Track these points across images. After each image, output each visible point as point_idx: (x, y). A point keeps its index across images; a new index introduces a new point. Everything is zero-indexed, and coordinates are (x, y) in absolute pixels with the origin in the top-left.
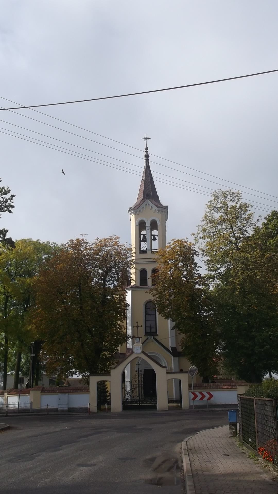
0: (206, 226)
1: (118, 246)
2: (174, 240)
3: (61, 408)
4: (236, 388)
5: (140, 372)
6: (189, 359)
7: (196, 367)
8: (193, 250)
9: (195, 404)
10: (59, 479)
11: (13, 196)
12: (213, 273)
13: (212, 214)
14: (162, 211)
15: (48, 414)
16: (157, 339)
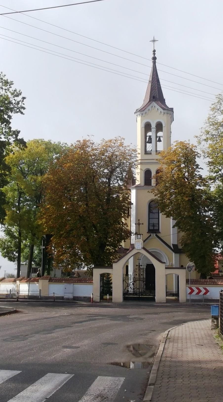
0: (209, 128)
1: (123, 147)
2: (177, 141)
3: (67, 296)
5: (140, 267)
6: (188, 256)
7: (193, 264)
8: (195, 152)
10: (42, 357)
11: (24, 98)
12: (214, 175)
13: (215, 116)
14: (168, 113)
15: (54, 301)
16: (159, 236)
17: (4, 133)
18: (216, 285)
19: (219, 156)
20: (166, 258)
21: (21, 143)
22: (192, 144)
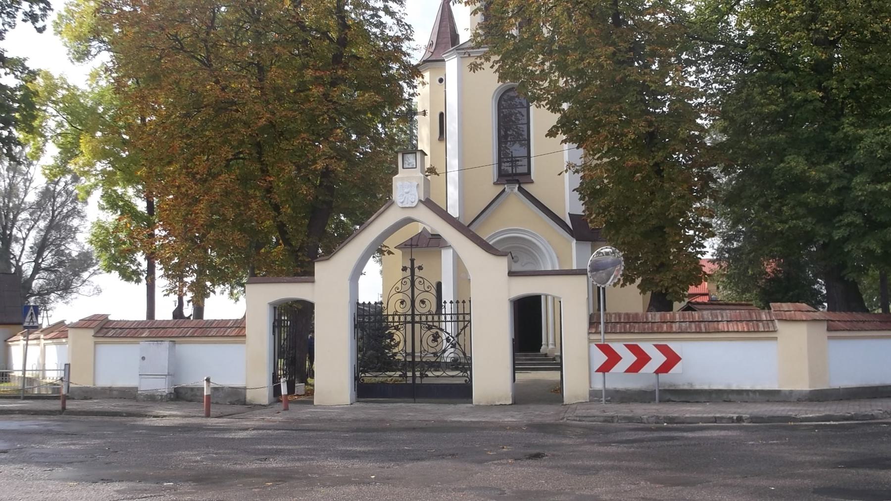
3: (147, 385)
4: (775, 331)
18: (706, 332)
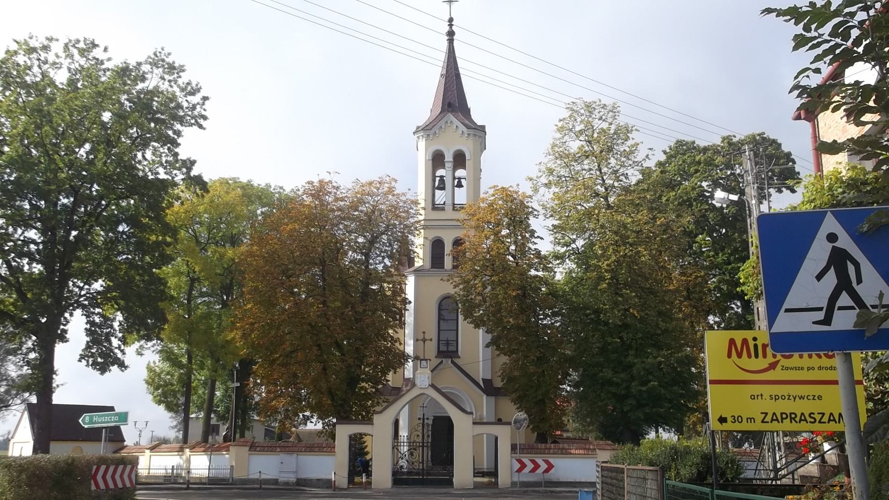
2: (494, 187)
3: (283, 478)
6: (514, 401)
7: (525, 415)
8: (528, 207)
9: (520, 480)
11: (205, 99)
12: (563, 250)
13: (565, 142)
14: (475, 135)
17: (165, 164)
19: (571, 216)
20: (469, 403)
21: (198, 182)
22: (523, 193)
